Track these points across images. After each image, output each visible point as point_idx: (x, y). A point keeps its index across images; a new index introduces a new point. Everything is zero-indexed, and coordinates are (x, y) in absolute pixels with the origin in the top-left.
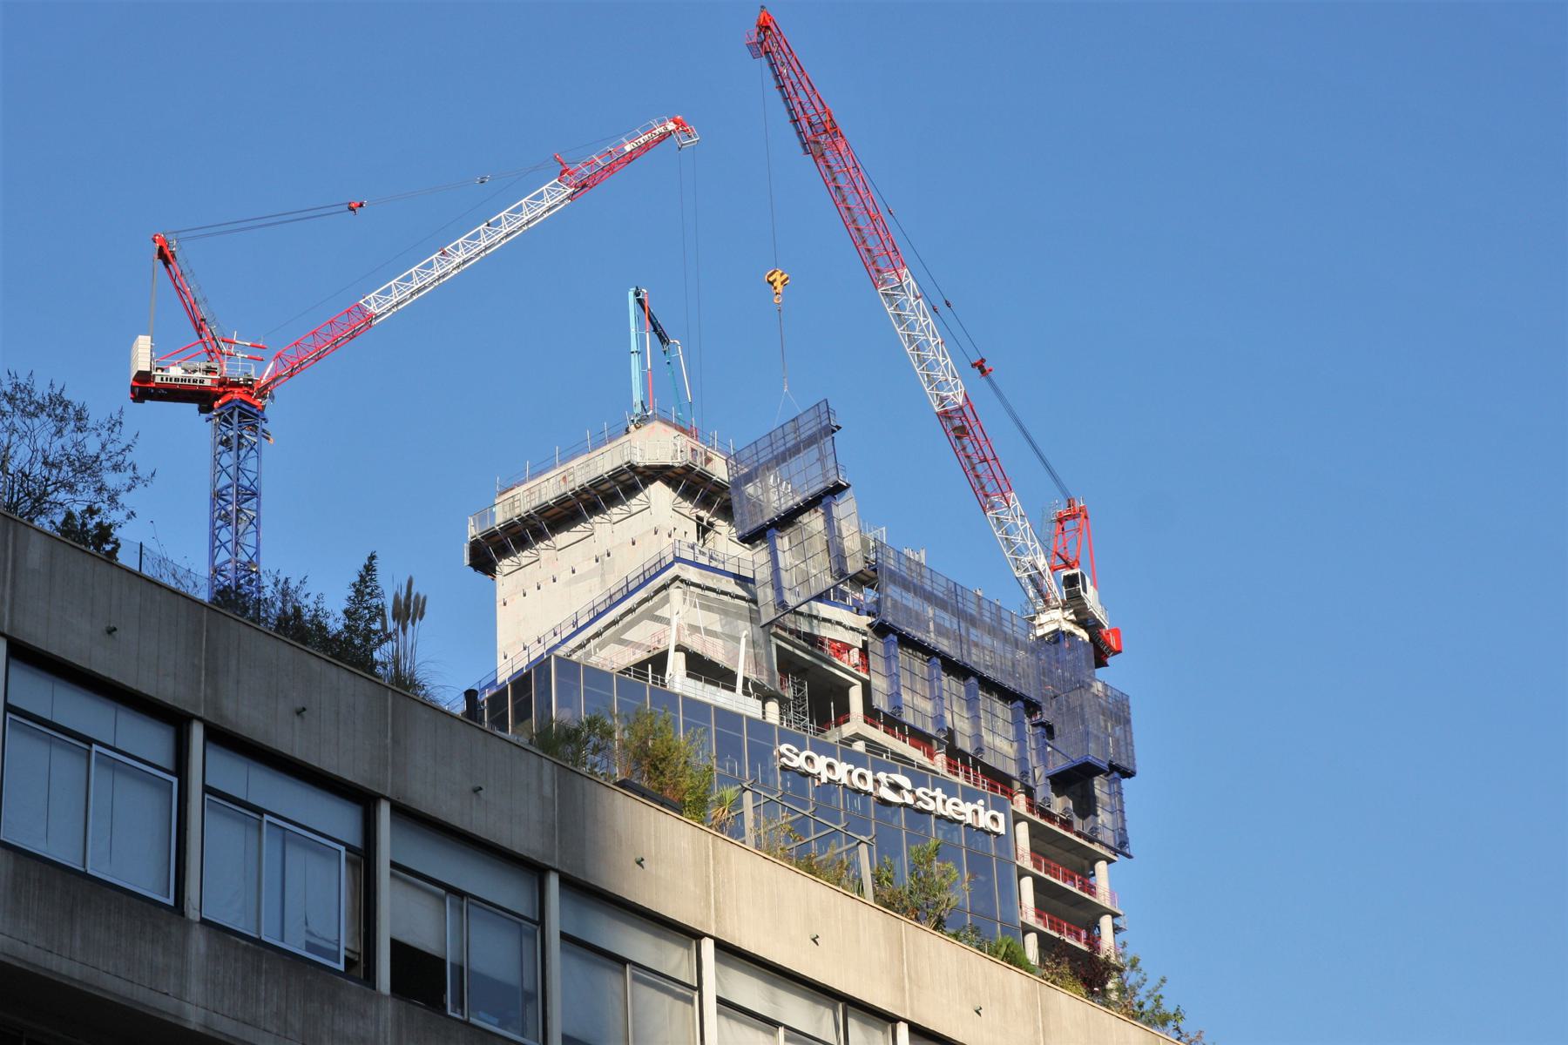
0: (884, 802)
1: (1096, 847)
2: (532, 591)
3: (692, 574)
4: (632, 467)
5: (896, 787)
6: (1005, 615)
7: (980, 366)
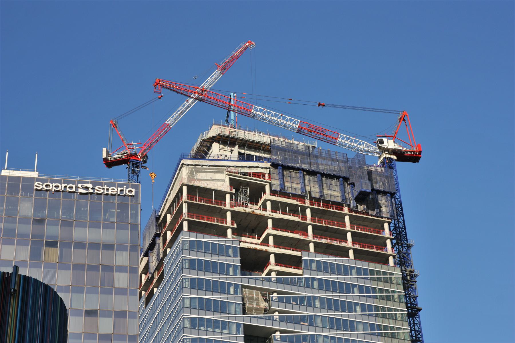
5: (87, 188)
6: (332, 153)
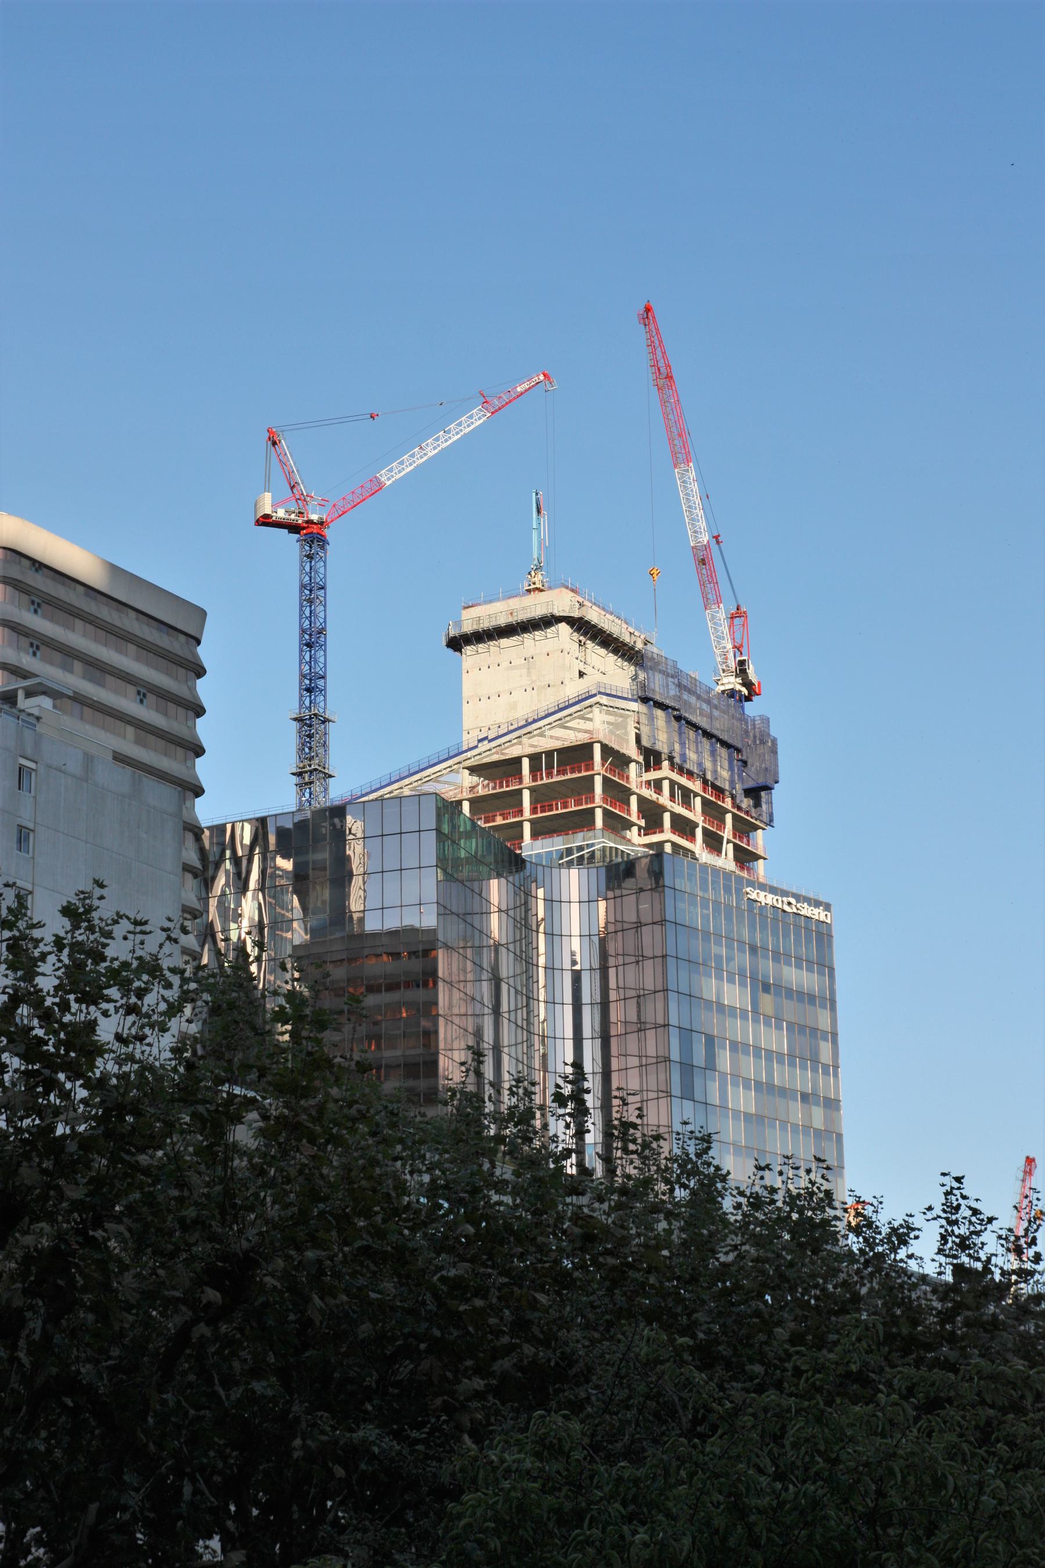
0: (784, 911)
1: (758, 823)
2: (484, 668)
3: (604, 700)
4: (553, 616)
5: (789, 904)
7: (716, 537)
